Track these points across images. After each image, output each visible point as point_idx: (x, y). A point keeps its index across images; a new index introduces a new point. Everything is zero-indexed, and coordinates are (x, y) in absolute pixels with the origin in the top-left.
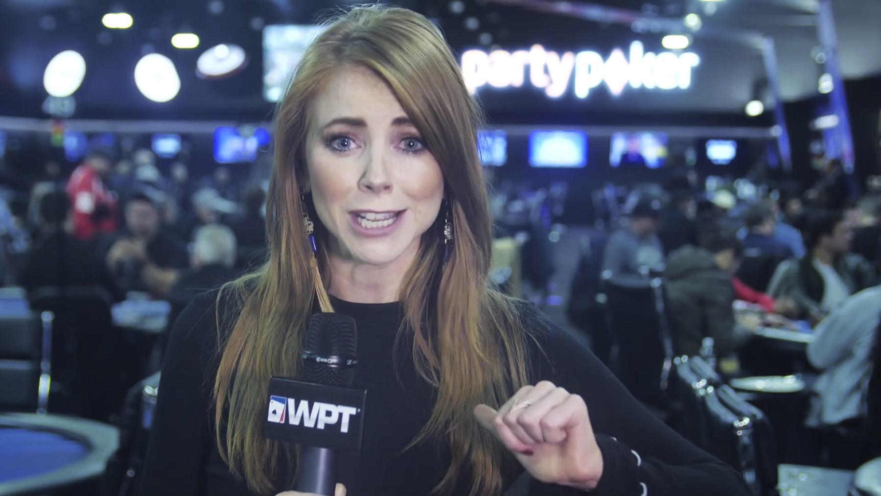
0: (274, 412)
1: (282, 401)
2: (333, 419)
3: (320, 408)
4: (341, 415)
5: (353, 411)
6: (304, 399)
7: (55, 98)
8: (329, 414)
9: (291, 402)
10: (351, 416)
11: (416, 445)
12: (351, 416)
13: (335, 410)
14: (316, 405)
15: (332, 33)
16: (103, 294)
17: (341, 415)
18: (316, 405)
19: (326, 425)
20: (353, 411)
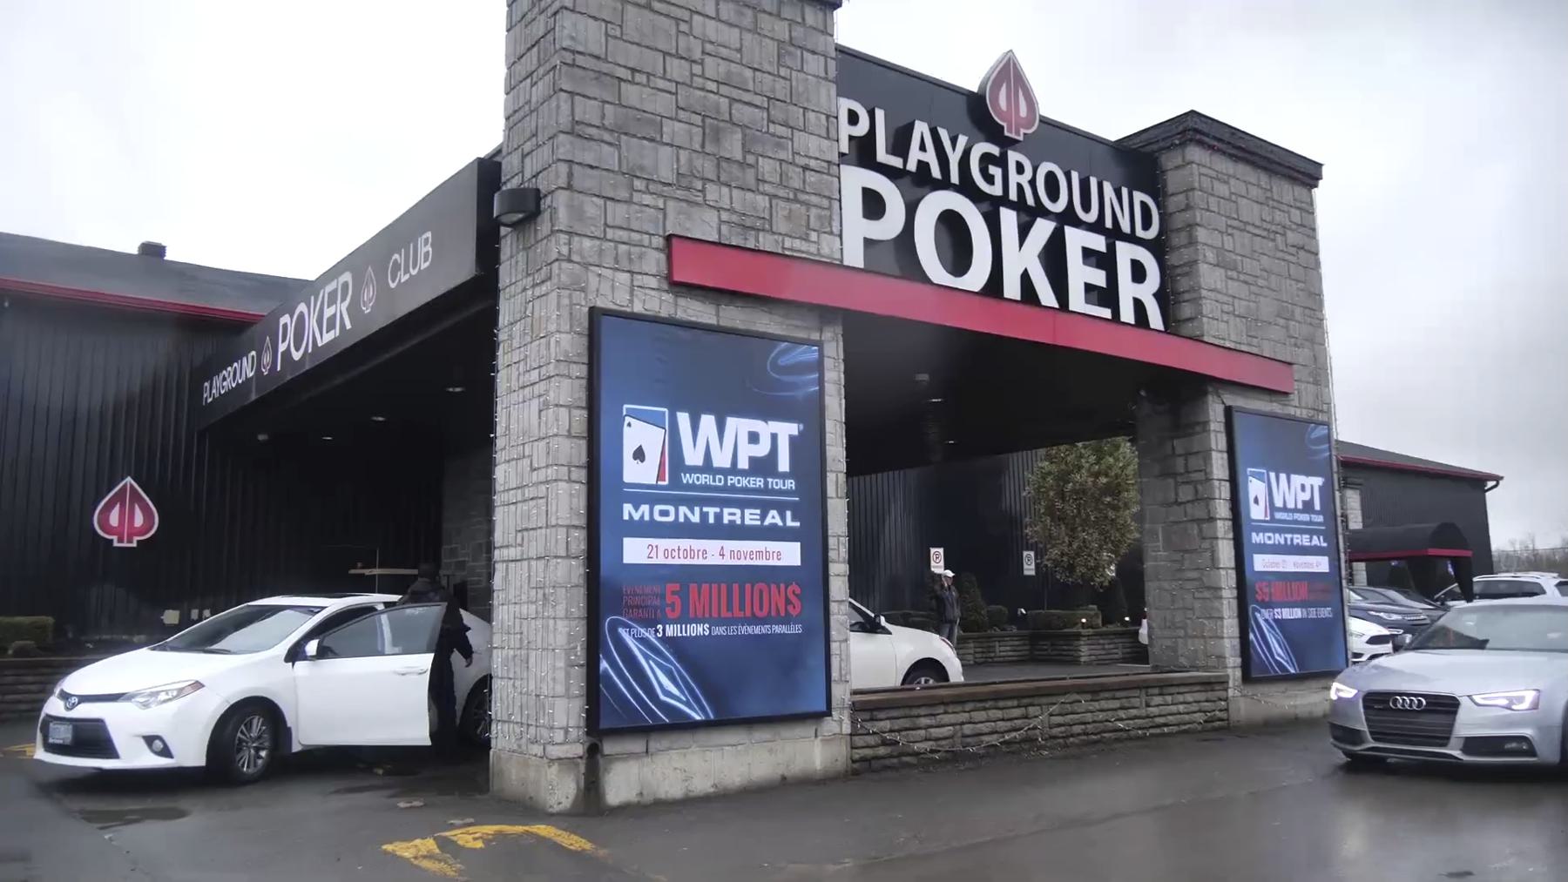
0: (639, 455)
1: (654, 420)
2: (762, 450)
3: (738, 426)
4: (774, 437)
5: (793, 428)
6: (709, 411)
7: (1308, 209)
8: (754, 438)
9: (683, 419)
10: (792, 439)
11: (1206, 455)
12: (792, 438)
13: (765, 428)
14: (731, 422)
15: (1428, 638)
16: (1322, 431)
17: (774, 437)
18: (731, 422)
19: (752, 460)
20: (793, 428)
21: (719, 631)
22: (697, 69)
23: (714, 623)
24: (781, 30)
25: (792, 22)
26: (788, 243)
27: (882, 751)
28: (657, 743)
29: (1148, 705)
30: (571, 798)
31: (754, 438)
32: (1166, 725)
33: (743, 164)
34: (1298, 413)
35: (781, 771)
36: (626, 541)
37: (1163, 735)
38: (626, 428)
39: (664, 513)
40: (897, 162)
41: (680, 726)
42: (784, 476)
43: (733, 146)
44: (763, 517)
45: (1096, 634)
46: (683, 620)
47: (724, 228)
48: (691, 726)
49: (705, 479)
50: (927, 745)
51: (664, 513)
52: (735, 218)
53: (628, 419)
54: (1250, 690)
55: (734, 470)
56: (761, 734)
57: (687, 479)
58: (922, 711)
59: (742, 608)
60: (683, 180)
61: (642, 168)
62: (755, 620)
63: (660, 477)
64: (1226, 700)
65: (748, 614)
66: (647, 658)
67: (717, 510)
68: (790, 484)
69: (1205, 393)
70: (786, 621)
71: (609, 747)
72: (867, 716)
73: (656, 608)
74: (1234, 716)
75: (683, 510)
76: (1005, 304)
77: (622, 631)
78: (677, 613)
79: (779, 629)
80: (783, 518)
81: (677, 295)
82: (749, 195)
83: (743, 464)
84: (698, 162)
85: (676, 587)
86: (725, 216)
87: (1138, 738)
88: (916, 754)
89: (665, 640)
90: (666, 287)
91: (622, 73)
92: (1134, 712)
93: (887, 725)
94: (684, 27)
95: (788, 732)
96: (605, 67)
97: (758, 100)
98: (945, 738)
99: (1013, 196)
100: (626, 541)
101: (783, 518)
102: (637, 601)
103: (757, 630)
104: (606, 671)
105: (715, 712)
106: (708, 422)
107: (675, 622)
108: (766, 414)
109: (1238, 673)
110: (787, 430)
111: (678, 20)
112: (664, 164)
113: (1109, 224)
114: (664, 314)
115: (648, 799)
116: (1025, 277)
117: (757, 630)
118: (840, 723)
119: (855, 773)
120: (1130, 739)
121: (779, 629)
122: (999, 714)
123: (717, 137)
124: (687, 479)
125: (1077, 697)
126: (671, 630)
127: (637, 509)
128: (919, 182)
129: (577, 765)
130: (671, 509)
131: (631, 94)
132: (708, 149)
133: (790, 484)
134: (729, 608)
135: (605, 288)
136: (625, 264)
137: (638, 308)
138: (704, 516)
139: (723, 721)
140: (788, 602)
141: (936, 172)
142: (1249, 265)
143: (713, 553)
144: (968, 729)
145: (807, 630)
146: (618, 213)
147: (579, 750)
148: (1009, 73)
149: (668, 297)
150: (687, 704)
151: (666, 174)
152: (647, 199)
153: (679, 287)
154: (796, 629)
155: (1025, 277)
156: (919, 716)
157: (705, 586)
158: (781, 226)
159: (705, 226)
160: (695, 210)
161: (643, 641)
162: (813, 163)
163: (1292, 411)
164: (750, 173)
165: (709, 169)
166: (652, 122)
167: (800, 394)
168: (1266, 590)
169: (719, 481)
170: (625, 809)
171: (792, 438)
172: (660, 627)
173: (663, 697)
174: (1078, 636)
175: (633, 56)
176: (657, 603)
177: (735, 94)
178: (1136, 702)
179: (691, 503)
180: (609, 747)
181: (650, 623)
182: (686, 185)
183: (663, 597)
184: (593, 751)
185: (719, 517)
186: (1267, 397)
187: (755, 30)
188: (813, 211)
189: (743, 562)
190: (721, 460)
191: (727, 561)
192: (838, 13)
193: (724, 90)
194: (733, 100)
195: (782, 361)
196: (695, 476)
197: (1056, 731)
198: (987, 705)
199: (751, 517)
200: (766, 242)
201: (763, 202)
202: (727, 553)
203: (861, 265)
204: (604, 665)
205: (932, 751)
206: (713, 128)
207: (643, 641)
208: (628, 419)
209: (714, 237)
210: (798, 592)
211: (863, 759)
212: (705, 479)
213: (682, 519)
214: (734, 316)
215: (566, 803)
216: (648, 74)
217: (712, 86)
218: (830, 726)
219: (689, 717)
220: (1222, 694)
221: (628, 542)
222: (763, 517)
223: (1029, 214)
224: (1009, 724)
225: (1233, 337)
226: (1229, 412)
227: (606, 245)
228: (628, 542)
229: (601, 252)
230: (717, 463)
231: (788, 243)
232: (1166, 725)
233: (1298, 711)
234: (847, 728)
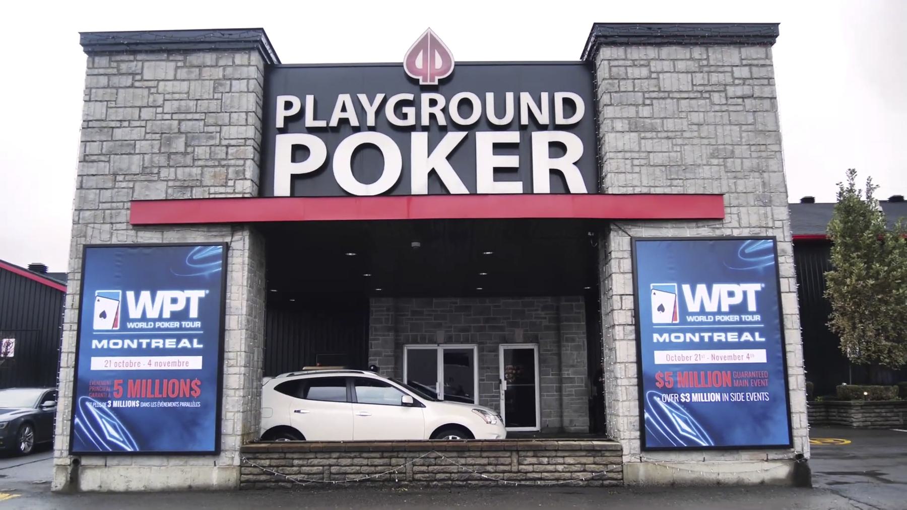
0: (661, 308)
2: (180, 306)
3: (721, 289)
4: (188, 300)
6: (701, 282)
8: (731, 294)
12: (757, 293)
17: (188, 300)
20: (758, 287)
21: (145, 405)
22: (159, 110)
23: (142, 400)
24: (218, 73)
25: (225, 67)
26: (212, 190)
27: (263, 477)
28: (111, 461)
29: (519, 464)
30: (63, 485)
31: (174, 301)
32: (541, 479)
33: (185, 154)
34: (736, 233)
35: (188, 483)
36: (201, 357)
37: (539, 486)
38: (96, 302)
39: (115, 344)
40: (322, 124)
41: (118, 453)
42: (752, 313)
43: (179, 145)
44: (740, 336)
45: (866, 405)
46: (124, 398)
47: (170, 191)
48: (697, 449)
49: (702, 318)
50: (299, 477)
51: (115, 344)
52: (178, 184)
53: (653, 291)
54: (646, 457)
55: (160, 319)
56: (174, 462)
57: (690, 319)
58: (295, 456)
59: (161, 393)
60: (145, 171)
61: (121, 170)
62: (165, 400)
63: (674, 318)
64: (621, 463)
65: (165, 396)
66: (101, 417)
67: (710, 334)
68: (757, 318)
69: (610, 230)
70: (189, 399)
71: (84, 461)
72: (250, 456)
73: (108, 393)
74: (629, 475)
75: (689, 335)
76: (413, 198)
77: (88, 404)
78: (120, 396)
79: (184, 404)
80: (753, 336)
81: (137, 231)
82: (187, 170)
83: (725, 308)
84: (156, 158)
85: (121, 381)
86: (171, 184)
87: (504, 486)
88: (289, 481)
89: (112, 409)
90: (131, 227)
91: (113, 124)
92: (502, 468)
93: (267, 462)
94: (153, 90)
95: (193, 461)
96: (104, 124)
97: (197, 116)
98: (314, 474)
99: (425, 121)
100: (201, 357)
101: (753, 336)
102: (98, 389)
103: (170, 404)
104: (648, 419)
105: (715, 442)
106: (701, 288)
107: (118, 399)
108: (182, 287)
109: (637, 444)
110: (753, 288)
111: (149, 88)
112: (135, 165)
113: (525, 120)
114: (129, 242)
115: (105, 488)
116: (433, 174)
117: (170, 404)
118: (231, 457)
119: (241, 489)
120: (497, 486)
121: (184, 404)
122: (365, 462)
123: (169, 142)
124: (690, 319)
125: (440, 454)
126: (116, 404)
127: (661, 336)
128: (331, 135)
129: (67, 469)
130: (681, 335)
131: (119, 134)
132: (163, 150)
133: (757, 318)
134: (153, 393)
135: (96, 232)
136: (108, 220)
137: (114, 241)
138: (702, 338)
139: (146, 451)
140: (191, 389)
141: (354, 122)
142: (670, 124)
143: (144, 363)
144: (334, 469)
145: (774, 399)
146: (107, 195)
147: (68, 461)
148: (429, 44)
149: (133, 232)
150: (123, 442)
151: (135, 169)
152: (124, 185)
153: (138, 227)
154: (197, 404)
155: (433, 174)
156: (293, 459)
157: (138, 381)
158: (207, 181)
159: (158, 191)
160: (152, 185)
161: (100, 409)
162: (233, 142)
163: (727, 232)
164: (189, 157)
165: (162, 160)
166: (129, 145)
167: (760, 267)
168: (672, 379)
169: (711, 319)
170: (91, 493)
171: (757, 293)
172: (110, 402)
173: (109, 438)
174: (850, 406)
175: (121, 114)
176: (109, 390)
177: (182, 116)
178: (502, 460)
179: (132, 338)
180: (84, 461)
181: (104, 400)
182: (148, 173)
183: (112, 386)
184: (76, 463)
185: (711, 338)
186: (694, 225)
187: (200, 78)
188: (231, 170)
189: (163, 368)
190: (711, 307)
191: (153, 368)
192: (775, 49)
193: (175, 116)
194: (180, 121)
195: (747, 251)
196: (135, 324)
197: (418, 476)
198: (352, 455)
199: (170, 343)
200: (197, 193)
201: (199, 170)
202: (153, 363)
203: (585, 191)
204: (647, 415)
205: (300, 481)
206: (166, 138)
207: (100, 409)
208: (653, 291)
209: (163, 197)
210: (199, 383)
211: (247, 481)
212: (702, 318)
213: (688, 340)
214: (172, 237)
215: (60, 487)
216: (129, 121)
217: (168, 117)
218: (224, 459)
219: (122, 448)
220: (618, 460)
221: (657, 353)
222: (740, 336)
223: (436, 132)
224: (373, 469)
225: (645, 183)
226: (634, 241)
227: (99, 212)
228: (657, 353)
229: (95, 216)
230: (707, 310)
231: (212, 190)
232: (541, 479)
233: (721, 477)
234: (237, 462)
